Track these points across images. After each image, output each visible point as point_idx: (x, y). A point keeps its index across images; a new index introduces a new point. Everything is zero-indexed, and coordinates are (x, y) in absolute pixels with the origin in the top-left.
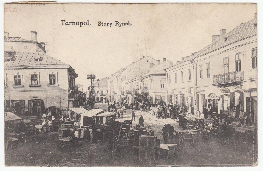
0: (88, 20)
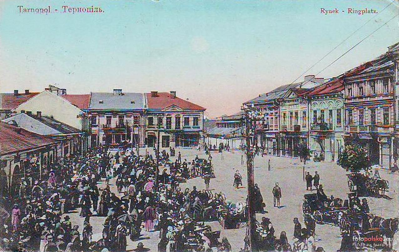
0: (49, 7)
